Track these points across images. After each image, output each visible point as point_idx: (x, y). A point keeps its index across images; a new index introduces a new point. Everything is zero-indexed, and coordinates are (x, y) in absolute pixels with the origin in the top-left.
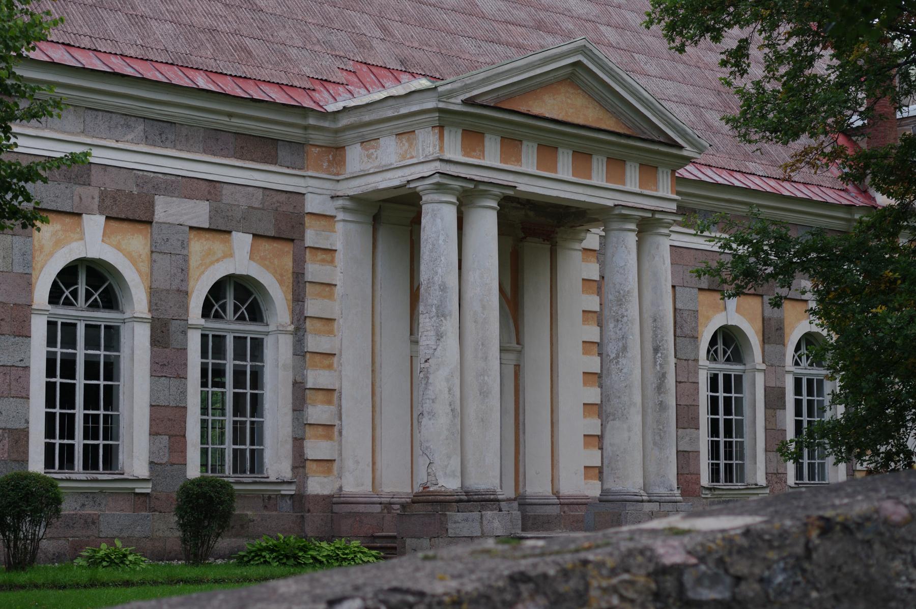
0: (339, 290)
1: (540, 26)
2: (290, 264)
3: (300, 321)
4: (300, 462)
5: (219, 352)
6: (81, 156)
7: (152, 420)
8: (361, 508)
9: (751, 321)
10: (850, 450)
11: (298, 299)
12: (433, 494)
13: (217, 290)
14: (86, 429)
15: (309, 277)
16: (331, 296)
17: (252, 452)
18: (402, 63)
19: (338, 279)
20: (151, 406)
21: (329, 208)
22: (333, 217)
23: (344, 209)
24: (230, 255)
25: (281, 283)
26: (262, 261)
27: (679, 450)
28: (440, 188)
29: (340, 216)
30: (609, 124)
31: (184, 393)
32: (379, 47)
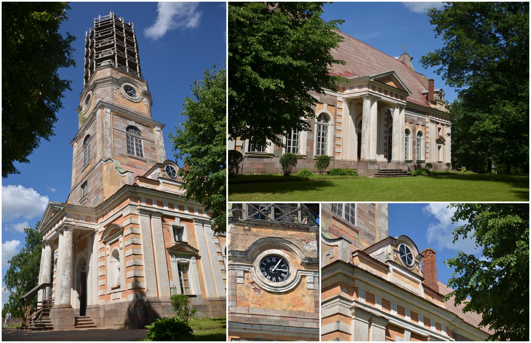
0: (343, 117)
1: (373, 68)
2: (334, 111)
3: (336, 122)
4: (334, 153)
5: (320, 128)
6: (325, 85)
7: (307, 142)
8: (346, 163)
9: (411, 128)
10: (41, 134)
11: (335, 118)
12: (365, 160)
13: (320, 115)
14: (293, 144)
15: (337, 114)
16: (341, 118)
17: (297, 148)
18: (353, 72)
19: (343, 115)
20: (308, 140)
21: (342, 100)
22: (342, 102)
23: (345, 101)
24: (323, 108)
25: (332, 114)
26: (329, 110)
27: (236, 145)
28: (368, 98)
29: (344, 102)
30: (396, 87)
31: (313, 137)
32: (349, 69)
